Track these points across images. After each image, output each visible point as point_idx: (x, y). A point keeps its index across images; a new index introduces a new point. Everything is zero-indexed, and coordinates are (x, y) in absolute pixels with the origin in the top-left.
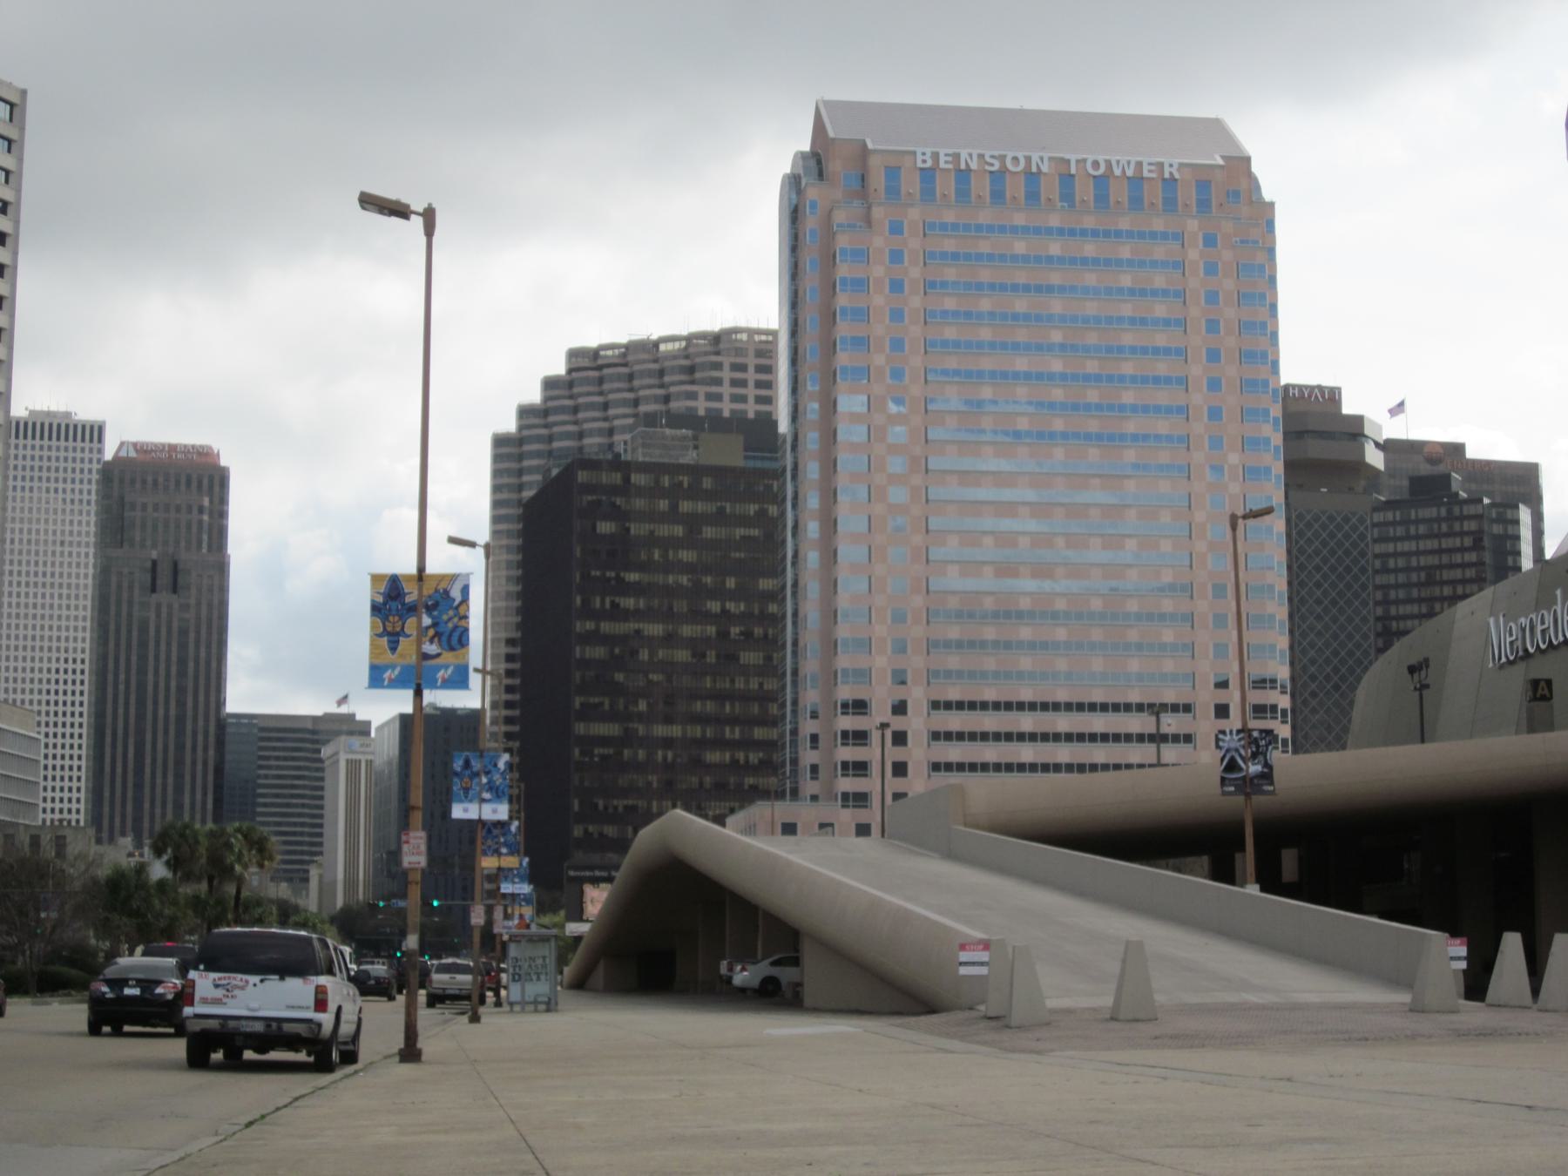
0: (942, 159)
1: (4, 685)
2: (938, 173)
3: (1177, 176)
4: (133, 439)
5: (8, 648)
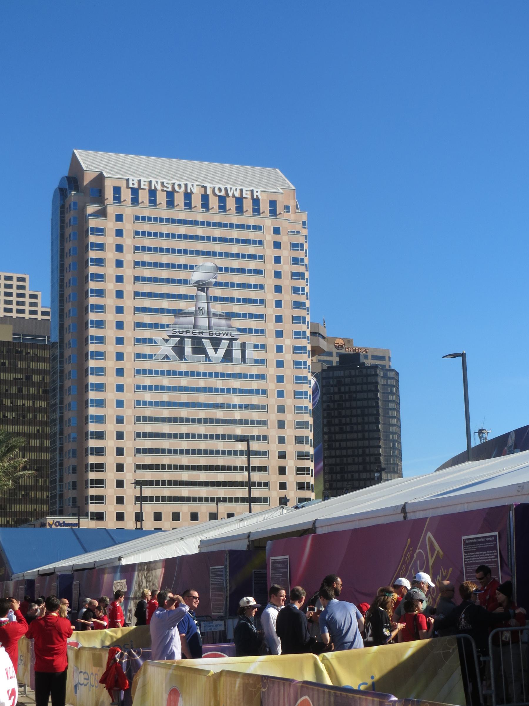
0: (142, 183)
2: (140, 191)
3: (260, 197)
4: (231, 549)
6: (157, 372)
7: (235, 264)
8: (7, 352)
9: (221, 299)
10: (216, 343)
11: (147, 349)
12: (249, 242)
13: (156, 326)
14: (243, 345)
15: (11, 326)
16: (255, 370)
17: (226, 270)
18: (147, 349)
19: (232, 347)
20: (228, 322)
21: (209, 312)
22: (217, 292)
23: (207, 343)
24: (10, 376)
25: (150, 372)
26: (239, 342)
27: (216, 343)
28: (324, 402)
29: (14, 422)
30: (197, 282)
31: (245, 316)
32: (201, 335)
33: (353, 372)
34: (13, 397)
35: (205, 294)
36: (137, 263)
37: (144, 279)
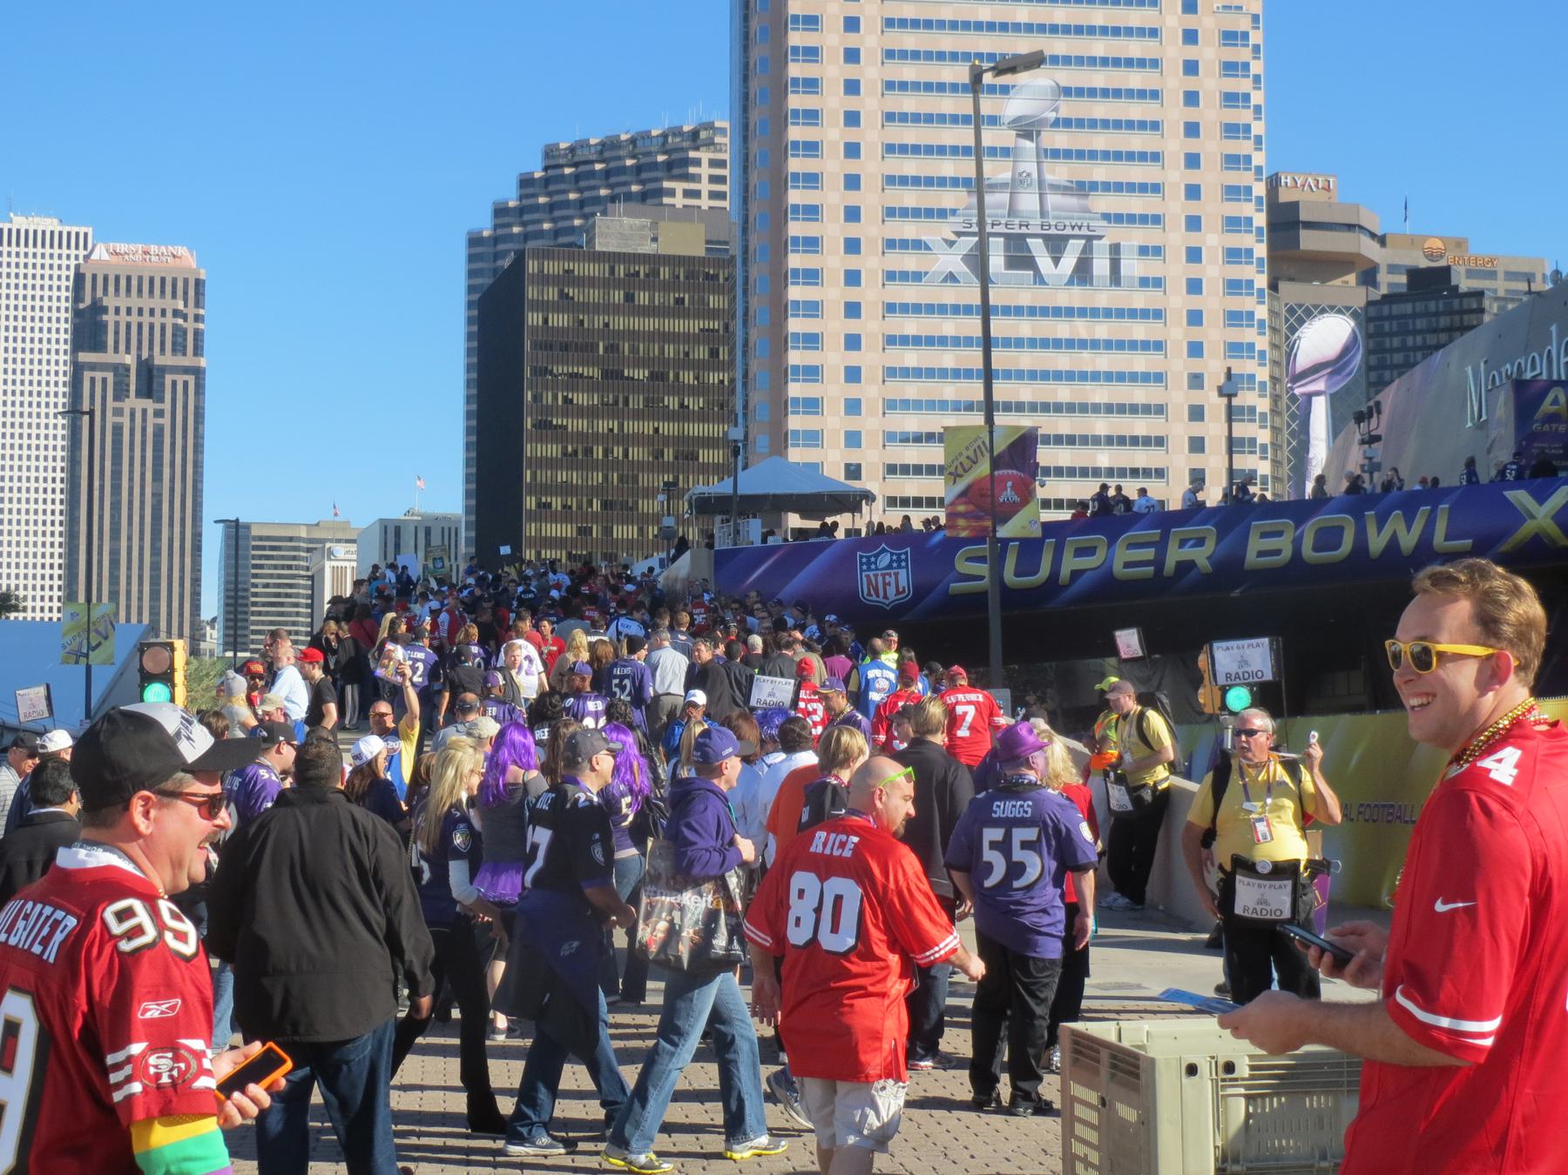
1: (4, 334)
5: (8, 286)
6: (930, 309)
7: (1099, 78)
8: (687, 277)
9: (1068, 154)
10: (1056, 245)
11: (909, 262)
12: (1129, 32)
13: (929, 213)
14: (1115, 249)
15: (702, 226)
16: (1140, 300)
17: (1080, 92)
18: (909, 262)
19: (1091, 252)
20: (1083, 202)
21: (1041, 182)
22: (1060, 139)
23: (1037, 247)
24: (695, 326)
25: (917, 309)
26: (1106, 242)
27: (1056, 245)
28: (1370, 368)
29: (702, 417)
30: (1014, 121)
31: (1118, 187)
32: (1024, 230)
33: (1432, 306)
34: (699, 366)
35: (1033, 145)
36: (890, 85)
37: (903, 117)
